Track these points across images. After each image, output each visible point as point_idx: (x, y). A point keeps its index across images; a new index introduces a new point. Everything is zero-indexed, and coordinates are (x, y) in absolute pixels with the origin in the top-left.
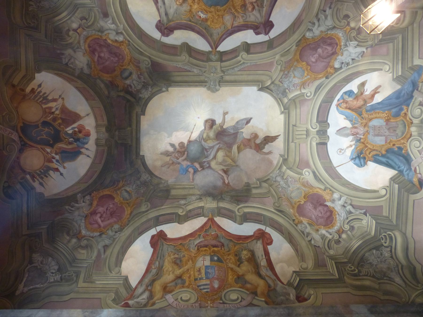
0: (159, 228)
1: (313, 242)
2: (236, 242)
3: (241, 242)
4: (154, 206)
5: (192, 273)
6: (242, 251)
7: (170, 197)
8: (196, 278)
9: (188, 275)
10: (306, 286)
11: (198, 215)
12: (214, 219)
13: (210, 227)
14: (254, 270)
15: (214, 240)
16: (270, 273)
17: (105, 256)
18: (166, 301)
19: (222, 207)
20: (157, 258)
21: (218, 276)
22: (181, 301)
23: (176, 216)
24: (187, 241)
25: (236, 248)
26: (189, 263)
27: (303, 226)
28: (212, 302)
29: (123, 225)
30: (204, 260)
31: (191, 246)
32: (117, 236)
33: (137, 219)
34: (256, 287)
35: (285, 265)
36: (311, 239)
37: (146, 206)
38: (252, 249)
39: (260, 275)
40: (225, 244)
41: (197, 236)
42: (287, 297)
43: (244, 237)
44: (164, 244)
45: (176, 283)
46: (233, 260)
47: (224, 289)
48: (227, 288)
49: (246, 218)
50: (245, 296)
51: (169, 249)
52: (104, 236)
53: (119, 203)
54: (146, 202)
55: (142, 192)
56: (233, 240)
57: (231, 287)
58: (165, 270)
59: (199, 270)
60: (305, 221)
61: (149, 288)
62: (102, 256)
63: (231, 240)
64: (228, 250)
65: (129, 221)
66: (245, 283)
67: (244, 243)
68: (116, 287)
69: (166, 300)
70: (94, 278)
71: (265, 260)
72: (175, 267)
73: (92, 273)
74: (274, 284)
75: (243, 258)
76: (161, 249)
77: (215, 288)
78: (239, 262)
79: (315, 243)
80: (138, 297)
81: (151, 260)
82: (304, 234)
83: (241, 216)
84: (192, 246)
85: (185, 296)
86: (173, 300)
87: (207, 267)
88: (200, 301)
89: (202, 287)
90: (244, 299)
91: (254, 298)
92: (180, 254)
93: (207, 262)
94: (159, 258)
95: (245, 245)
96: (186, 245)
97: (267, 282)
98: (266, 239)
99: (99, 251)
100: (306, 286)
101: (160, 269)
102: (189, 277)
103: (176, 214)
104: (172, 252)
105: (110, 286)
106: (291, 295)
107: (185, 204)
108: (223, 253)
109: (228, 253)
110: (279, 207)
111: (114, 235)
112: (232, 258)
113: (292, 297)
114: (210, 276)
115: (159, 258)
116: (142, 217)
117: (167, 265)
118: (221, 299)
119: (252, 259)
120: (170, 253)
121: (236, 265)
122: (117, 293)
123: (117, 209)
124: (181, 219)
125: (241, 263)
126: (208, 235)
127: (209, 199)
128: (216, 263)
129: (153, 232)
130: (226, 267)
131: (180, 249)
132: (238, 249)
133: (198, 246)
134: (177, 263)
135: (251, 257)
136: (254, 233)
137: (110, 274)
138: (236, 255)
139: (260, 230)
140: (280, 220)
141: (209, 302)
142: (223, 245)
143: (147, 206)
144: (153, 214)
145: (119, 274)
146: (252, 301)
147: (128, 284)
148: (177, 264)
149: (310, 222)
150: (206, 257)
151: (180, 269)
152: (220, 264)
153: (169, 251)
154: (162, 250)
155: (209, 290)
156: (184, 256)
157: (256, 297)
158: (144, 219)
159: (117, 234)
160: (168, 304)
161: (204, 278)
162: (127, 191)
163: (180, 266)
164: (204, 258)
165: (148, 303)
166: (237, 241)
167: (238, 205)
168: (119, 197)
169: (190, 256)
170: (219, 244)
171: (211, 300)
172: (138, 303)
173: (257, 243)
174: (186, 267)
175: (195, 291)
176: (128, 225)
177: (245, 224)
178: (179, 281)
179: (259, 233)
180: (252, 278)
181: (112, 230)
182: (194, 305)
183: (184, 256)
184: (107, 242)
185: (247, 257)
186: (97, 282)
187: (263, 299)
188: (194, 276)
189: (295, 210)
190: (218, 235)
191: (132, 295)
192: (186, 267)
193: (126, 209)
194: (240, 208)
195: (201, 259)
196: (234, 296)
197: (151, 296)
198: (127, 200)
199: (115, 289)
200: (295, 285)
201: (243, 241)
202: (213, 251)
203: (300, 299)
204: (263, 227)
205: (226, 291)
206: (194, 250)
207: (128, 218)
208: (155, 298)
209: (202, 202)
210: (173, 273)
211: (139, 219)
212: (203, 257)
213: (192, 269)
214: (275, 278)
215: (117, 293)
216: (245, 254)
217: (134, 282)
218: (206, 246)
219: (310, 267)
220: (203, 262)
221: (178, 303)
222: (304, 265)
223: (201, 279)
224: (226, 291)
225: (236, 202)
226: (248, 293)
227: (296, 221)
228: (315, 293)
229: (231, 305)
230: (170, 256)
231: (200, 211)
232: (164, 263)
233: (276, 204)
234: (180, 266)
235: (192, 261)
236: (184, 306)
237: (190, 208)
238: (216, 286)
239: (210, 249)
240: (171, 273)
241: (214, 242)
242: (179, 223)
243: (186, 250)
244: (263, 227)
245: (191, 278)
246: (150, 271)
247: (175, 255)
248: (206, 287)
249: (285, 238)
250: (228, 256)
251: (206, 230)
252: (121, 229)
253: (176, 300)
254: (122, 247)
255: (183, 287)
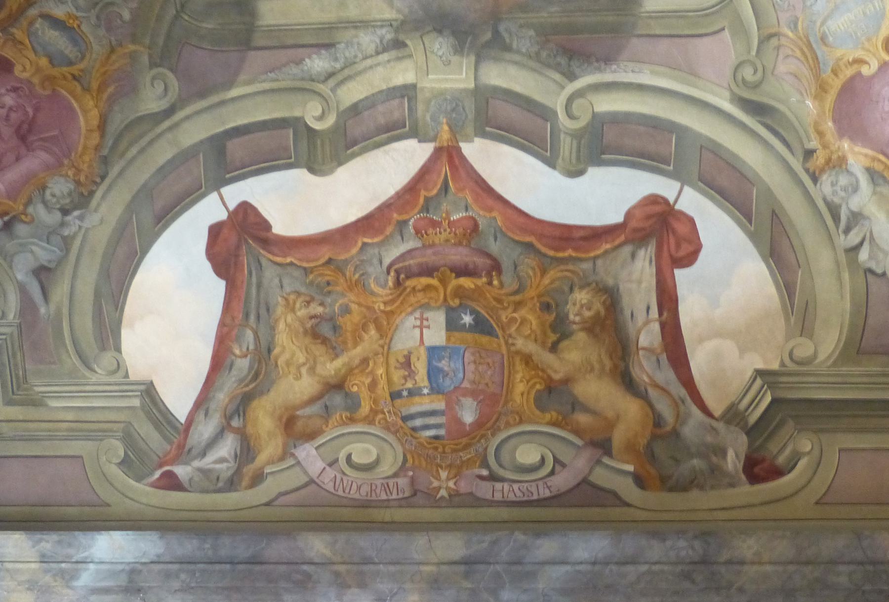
0: (237, 193)
1: (864, 255)
2: (551, 253)
3: (569, 252)
4: (199, 89)
5: (381, 371)
6: (571, 290)
7: (259, 40)
8: (397, 388)
9: (368, 381)
10: (791, 423)
11: (393, 131)
12: (459, 150)
13: (445, 187)
14: (608, 364)
15: (460, 244)
16: (667, 376)
17: (52, 307)
18: (297, 469)
19: (496, 90)
20: (247, 315)
21: (474, 382)
22: (348, 470)
23: (295, 134)
24: (354, 251)
25: (546, 281)
26: (366, 337)
27: (843, 180)
28: (453, 472)
29: (82, 179)
30: (421, 328)
31: (370, 270)
32: (74, 229)
33: (134, 151)
34: (611, 425)
35: (729, 347)
36: (861, 244)
37: (160, 87)
38: (610, 282)
39: (628, 383)
40: (506, 264)
41: (389, 230)
42: (714, 459)
43: (582, 233)
44: (264, 262)
45: (326, 407)
46: (534, 327)
47: (495, 431)
48: (508, 425)
49: (602, 144)
50: (566, 454)
51: (286, 281)
52: (21, 229)
53: (36, 80)
54: (153, 65)
55: (127, 15)
56: (539, 245)
57: (521, 422)
58: (281, 362)
59: (407, 363)
60: (857, 156)
61: (235, 423)
62: (43, 310)
63: (529, 246)
64: (515, 286)
65: (105, 161)
66: (573, 409)
67: (581, 260)
68: (121, 417)
69: (299, 463)
70: (36, 389)
71: (656, 327)
72: (319, 350)
73: (25, 371)
74: (678, 416)
75: (571, 317)
76: (254, 279)
77: (464, 424)
78: (558, 331)
79: (871, 257)
80: (203, 454)
81: (222, 324)
82: (836, 218)
83: (577, 135)
84: (374, 270)
85: (363, 451)
86: (320, 464)
87: (433, 351)
88: (413, 468)
89: (418, 422)
90: (564, 465)
91: (599, 462)
92: (329, 300)
93: (436, 335)
94: (252, 318)
95: (586, 266)
96: (350, 269)
97: (651, 406)
98: (672, 241)
99: (22, 289)
100: (791, 423)
101: (264, 354)
102: (373, 386)
103: (296, 124)
104: (298, 294)
105: (100, 416)
106: (731, 454)
107: (330, 75)
108: (495, 299)
109: (518, 298)
110: (756, 86)
111: (63, 224)
112: (530, 317)
113: (733, 461)
114: (448, 384)
115: (252, 318)
116: (151, 143)
117: (288, 345)
118: (485, 464)
119: (610, 324)
120: (292, 297)
121: (543, 344)
122: (129, 438)
123: (37, 109)
124: (318, 152)
125: (565, 335)
126: (435, 224)
127: (440, 45)
128: (469, 336)
129: (210, 210)
130: (504, 351)
131: (328, 284)
132: (557, 284)
133: (398, 272)
134: (323, 334)
135: (603, 312)
136: (629, 215)
137: (87, 373)
138: (546, 307)
139: (654, 200)
140: (750, 154)
141: (444, 474)
142: (496, 267)
143: (166, 90)
144: (196, 129)
145: (121, 373)
146: (590, 472)
147: (160, 411)
148: (325, 341)
149: (878, 167)
150: (428, 314)
151: (337, 356)
152: (484, 339)
153: (287, 289)
154: (259, 285)
155: (442, 432)
156: (346, 310)
157: (606, 460)
158: (163, 153)
159: (69, 218)
160: (306, 479)
161: (426, 391)
162: (56, 23)
163: (334, 348)
164: (422, 319)
165: (238, 472)
166: (556, 249)
167: (571, 77)
168: (32, 56)
169: (369, 308)
170: (481, 261)
171: (450, 466)
172: (205, 473)
173: (633, 256)
174: (357, 353)
175: (395, 433)
176: (103, 178)
177: (594, 173)
178: (338, 399)
179: (649, 217)
180: (598, 391)
181: (45, 203)
182: (391, 482)
183: (346, 310)
184: (43, 253)
185: (587, 314)
186: (54, 403)
187: (630, 468)
188: (389, 381)
189: (830, 99)
190: (476, 225)
191: (181, 446)
192: (357, 353)
193: (75, 105)
194: (579, 94)
195: (411, 321)
196: (528, 454)
197: (247, 451)
198: (70, 63)
199: (122, 425)
200: (753, 418)
201: (576, 249)
202: (459, 292)
203: (758, 469)
204: (664, 187)
205: (503, 435)
206: (381, 290)
207: (97, 148)
208: (262, 458)
209: (408, 64)
210: (312, 370)
211: (142, 151)
212: (417, 314)
213: (381, 359)
214: (683, 392)
215: (129, 438)
216: (580, 303)
217: (179, 401)
218: (428, 271)
219: (821, 357)
220: (423, 331)
221: (339, 476)
222: (805, 349)
223: (411, 393)
224: (503, 435)
225: (563, 61)
226: (579, 442)
227: (820, 158)
228: (816, 452)
229: (516, 486)
230: (293, 310)
231: (396, 109)
232: (273, 337)
233: (748, 73)
234: (334, 348)
235: (379, 328)
236: (359, 488)
237: (353, 92)
238: (468, 417)
239: (444, 282)
240: (304, 370)
241: (459, 255)
242: (312, 170)
243: (353, 286)
244: (664, 187)
245: (379, 391)
246: (228, 362)
247: (312, 305)
248: (432, 421)
249: (753, 237)
250: (515, 311)
251: (427, 199)
252: (82, 200)
253: (333, 463)
254: (105, 273)
255: (352, 420)
